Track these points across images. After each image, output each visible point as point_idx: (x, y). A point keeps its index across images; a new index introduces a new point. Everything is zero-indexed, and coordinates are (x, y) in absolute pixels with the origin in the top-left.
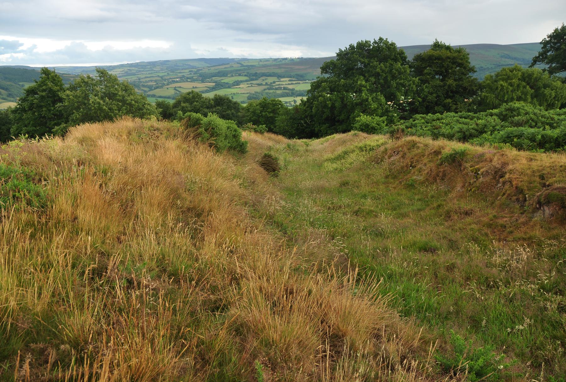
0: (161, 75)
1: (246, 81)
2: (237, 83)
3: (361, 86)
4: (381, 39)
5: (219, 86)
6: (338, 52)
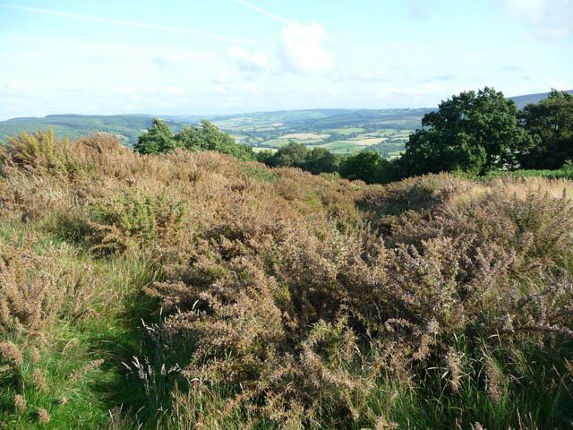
0: (277, 125)
1: (364, 133)
2: (354, 135)
3: (461, 137)
4: (486, 89)
5: (334, 138)
6: (440, 103)
